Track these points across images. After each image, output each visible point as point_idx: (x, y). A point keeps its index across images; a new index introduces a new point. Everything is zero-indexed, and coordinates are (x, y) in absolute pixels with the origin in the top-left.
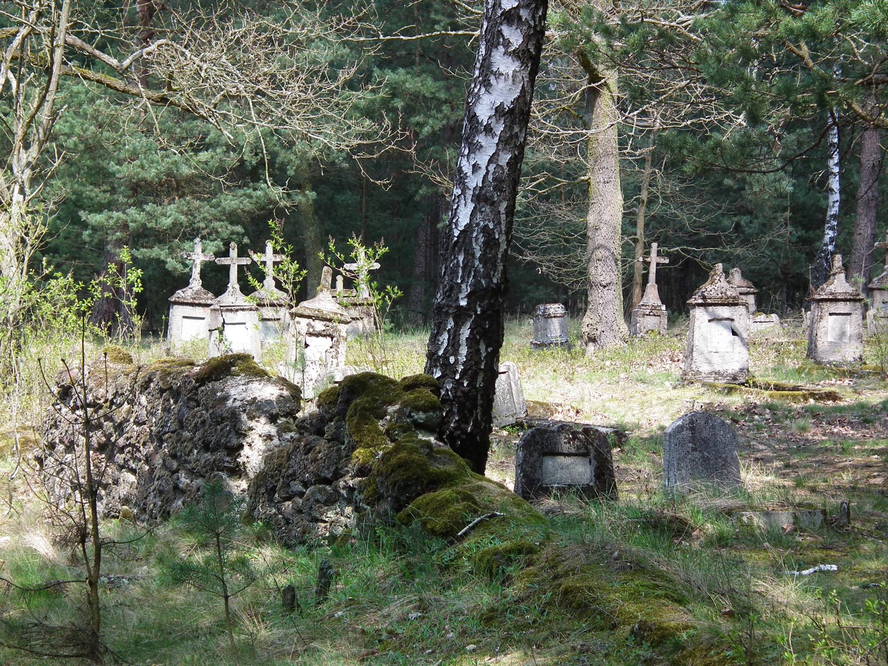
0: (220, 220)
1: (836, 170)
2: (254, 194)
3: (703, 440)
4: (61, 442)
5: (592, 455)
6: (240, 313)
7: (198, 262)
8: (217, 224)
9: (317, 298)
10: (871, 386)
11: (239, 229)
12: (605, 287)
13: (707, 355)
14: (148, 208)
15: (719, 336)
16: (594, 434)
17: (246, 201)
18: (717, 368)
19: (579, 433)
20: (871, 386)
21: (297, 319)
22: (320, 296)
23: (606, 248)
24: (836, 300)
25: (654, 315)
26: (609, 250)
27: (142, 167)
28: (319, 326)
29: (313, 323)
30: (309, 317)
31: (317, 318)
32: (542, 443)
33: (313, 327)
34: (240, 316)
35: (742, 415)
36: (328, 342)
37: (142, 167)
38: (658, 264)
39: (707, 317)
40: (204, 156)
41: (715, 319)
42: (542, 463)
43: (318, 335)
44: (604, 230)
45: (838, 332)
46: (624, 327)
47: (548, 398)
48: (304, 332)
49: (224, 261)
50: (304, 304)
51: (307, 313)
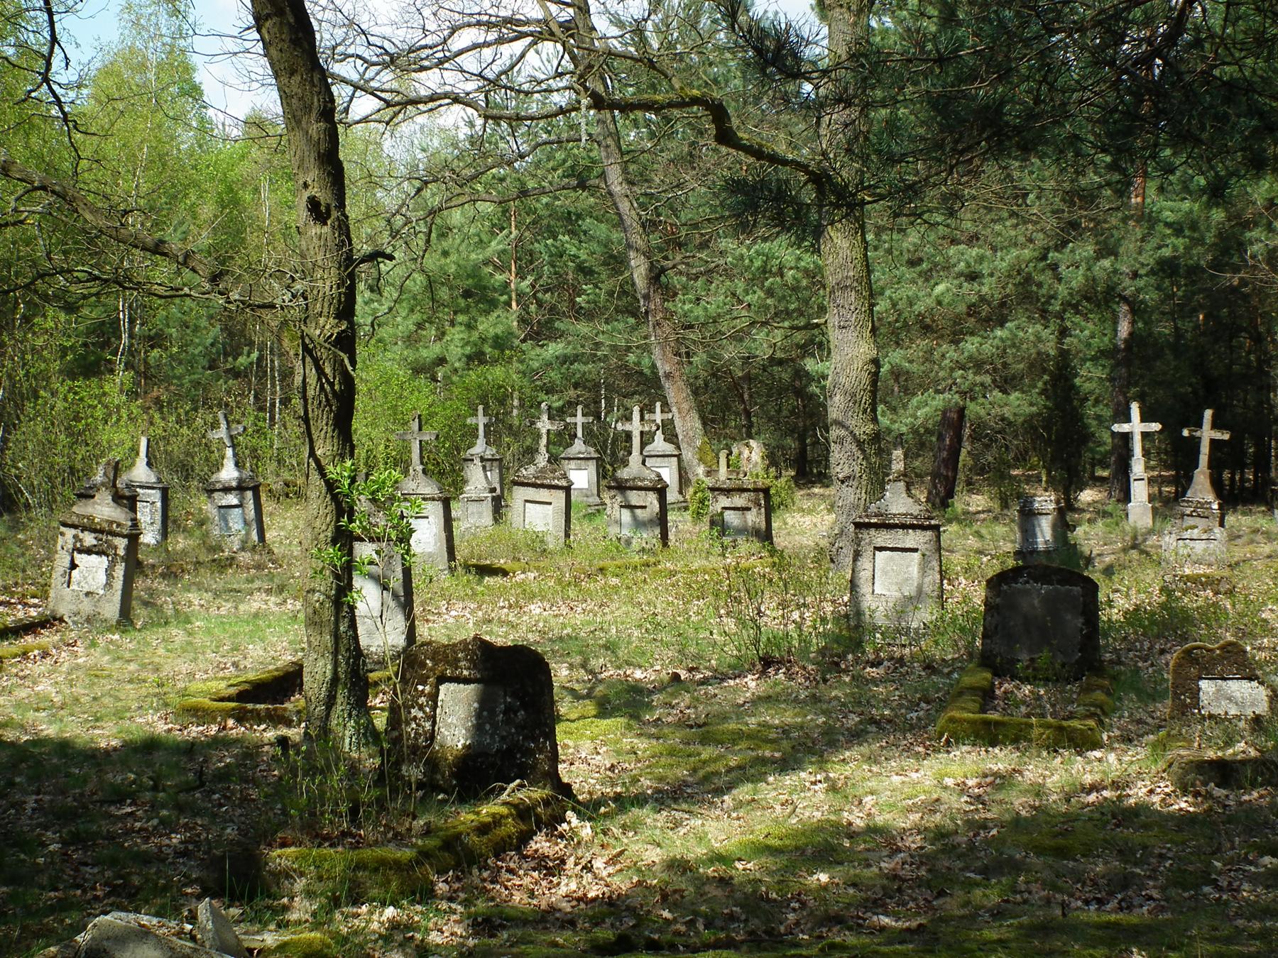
7: (544, 431)
12: (843, 482)
25: (1199, 516)
26: (847, 428)
28: (89, 539)
29: (81, 535)
31: (84, 529)
33: (81, 540)
36: (103, 562)
38: (1213, 441)
43: (89, 551)
51: (75, 520)
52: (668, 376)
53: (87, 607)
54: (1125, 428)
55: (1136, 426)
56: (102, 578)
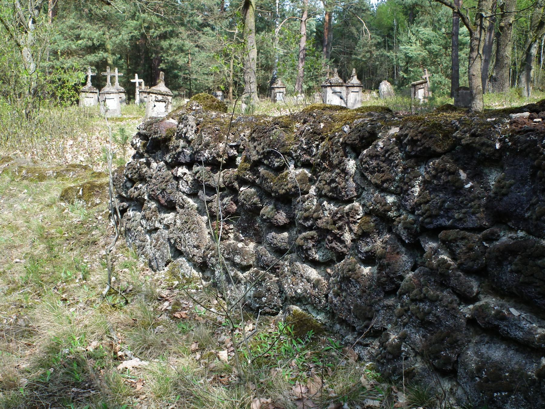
0: (87, 65)
2: (98, 55)
4: (152, 198)
6: (112, 94)
9: (158, 85)
17: (96, 58)
21: (151, 94)
22: (160, 84)
24: (354, 86)
27: (58, 45)
28: (160, 97)
30: (156, 93)
34: (112, 96)
37: (58, 45)
39: (332, 92)
40: (80, 42)
41: (335, 92)
45: (354, 99)
48: (154, 100)
50: (153, 88)
51: (155, 92)
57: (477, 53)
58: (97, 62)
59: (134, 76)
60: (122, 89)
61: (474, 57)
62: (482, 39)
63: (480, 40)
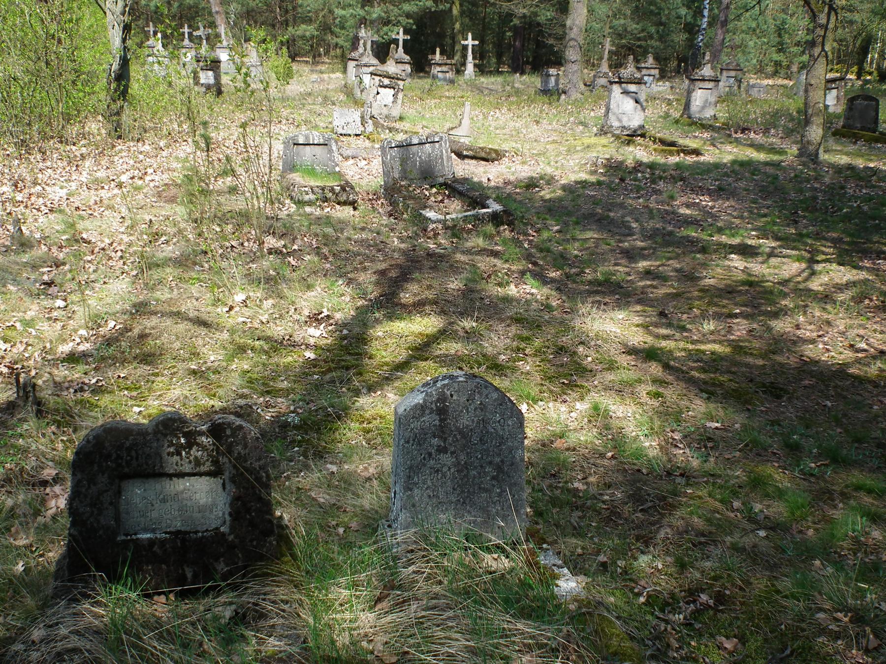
1: (707, 6)
3: (461, 432)
5: (227, 474)
8: (400, 18)
10: (722, 140)
11: (411, 21)
13: (620, 116)
14: (366, 8)
15: (628, 104)
16: (233, 435)
18: (626, 124)
19: (201, 434)
20: (722, 140)
23: (576, 41)
24: (704, 80)
28: (386, 81)
30: (380, 76)
31: (385, 76)
32: (119, 457)
35: (629, 172)
36: (392, 92)
41: (626, 92)
42: (119, 493)
43: (385, 87)
44: (575, 29)
45: (704, 99)
46: (65, 348)
47: (503, 146)
49: (397, 37)
51: (379, 73)
52: (217, 12)
53: (385, 111)
54: (466, 43)
55: (470, 42)
56: (391, 99)
57: (820, 49)
58: (417, 13)
59: (467, 35)
60: (407, 58)
61: (816, 55)
62: (831, 26)
63: (826, 29)
